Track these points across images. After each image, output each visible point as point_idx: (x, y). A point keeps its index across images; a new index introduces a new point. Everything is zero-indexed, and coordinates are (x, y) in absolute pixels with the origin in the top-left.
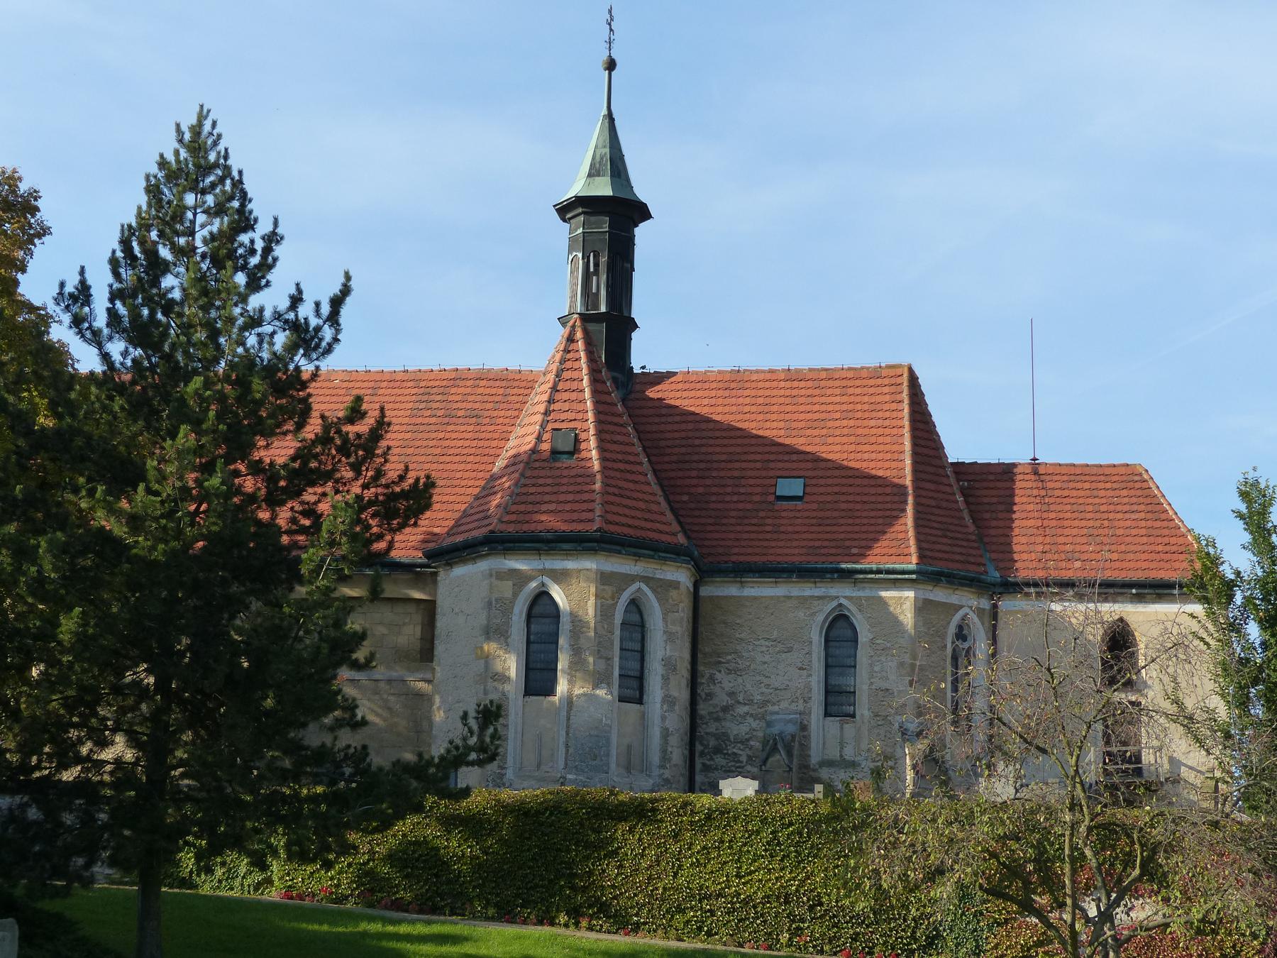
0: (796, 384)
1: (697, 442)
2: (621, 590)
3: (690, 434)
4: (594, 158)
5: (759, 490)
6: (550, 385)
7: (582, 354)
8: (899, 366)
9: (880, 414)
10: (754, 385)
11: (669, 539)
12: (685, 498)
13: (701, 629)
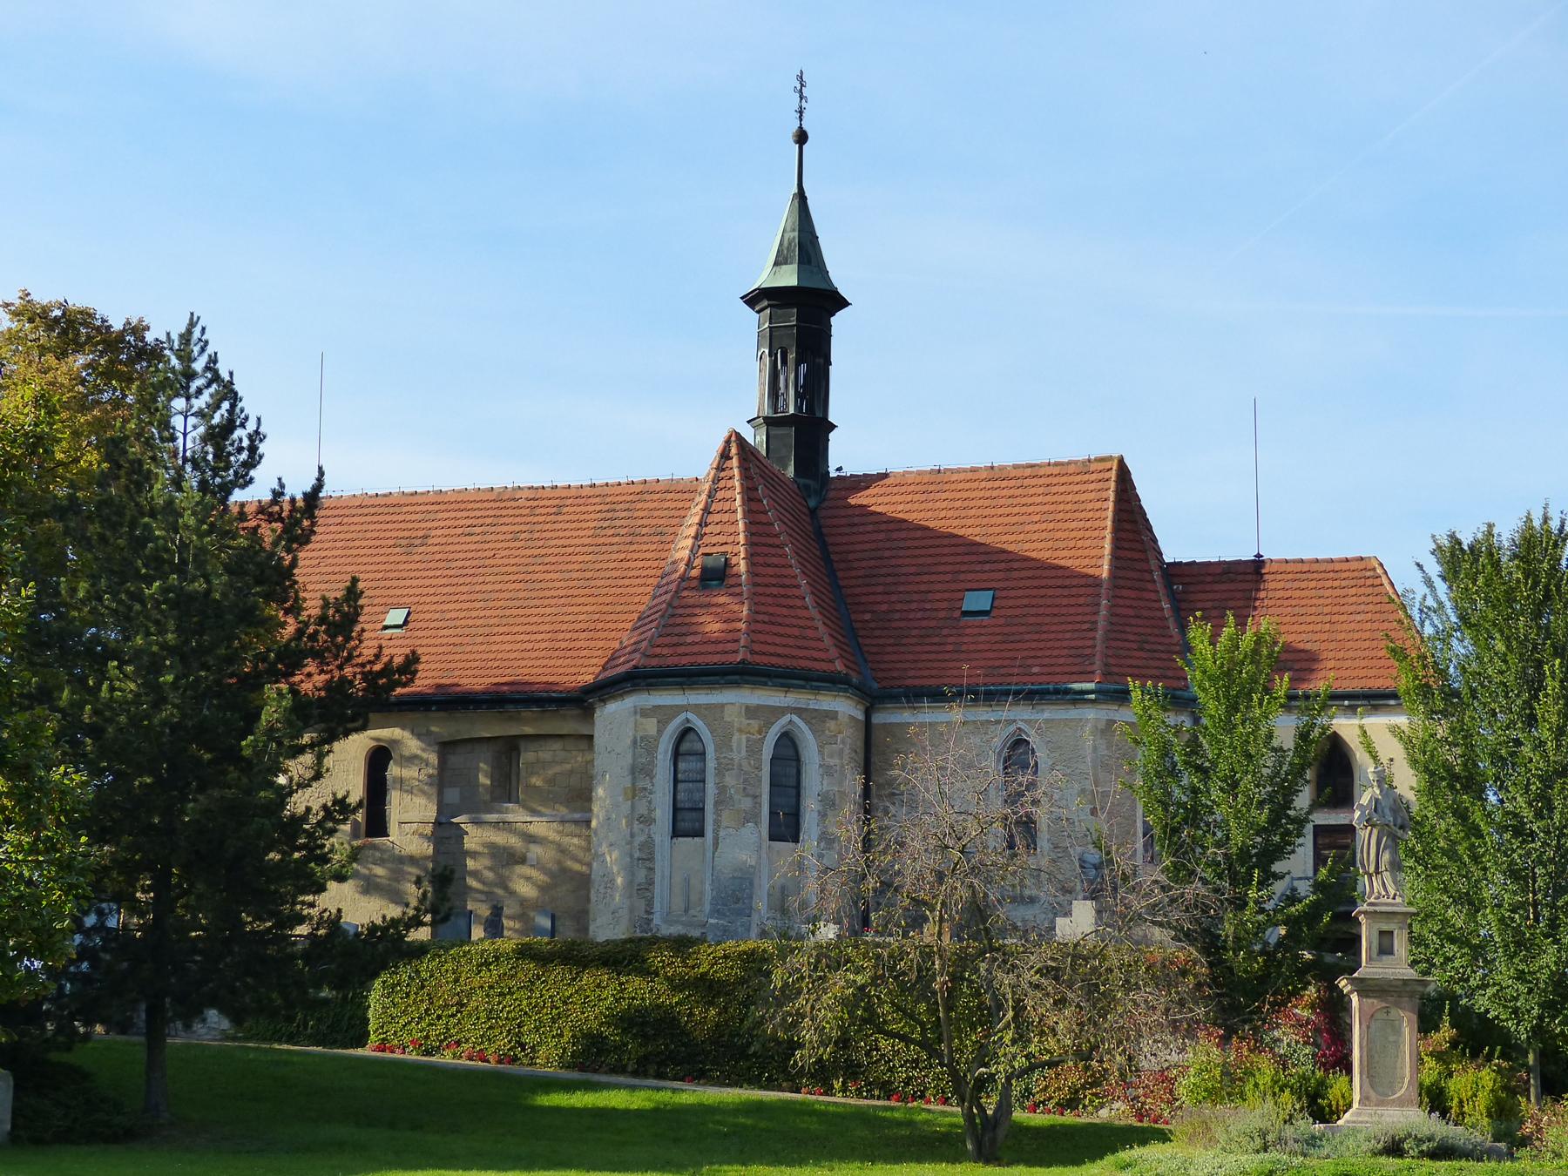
0: (997, 484)
1: (887, 554)
2: (769, 724)
3: (881, 545)
4: (781, 244)
5: (945, 605)
6: (701, 506)
7: (736, 471)
8: (1110, 458)
9: (1083, 515)
10: (953, 486)
11: (824, 666)
12: (868, 617)
13: (874, 759)
